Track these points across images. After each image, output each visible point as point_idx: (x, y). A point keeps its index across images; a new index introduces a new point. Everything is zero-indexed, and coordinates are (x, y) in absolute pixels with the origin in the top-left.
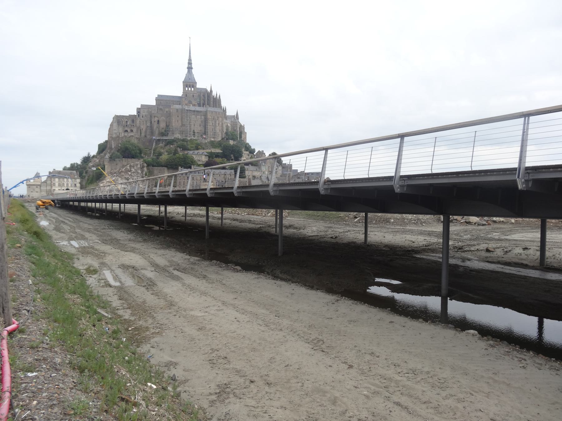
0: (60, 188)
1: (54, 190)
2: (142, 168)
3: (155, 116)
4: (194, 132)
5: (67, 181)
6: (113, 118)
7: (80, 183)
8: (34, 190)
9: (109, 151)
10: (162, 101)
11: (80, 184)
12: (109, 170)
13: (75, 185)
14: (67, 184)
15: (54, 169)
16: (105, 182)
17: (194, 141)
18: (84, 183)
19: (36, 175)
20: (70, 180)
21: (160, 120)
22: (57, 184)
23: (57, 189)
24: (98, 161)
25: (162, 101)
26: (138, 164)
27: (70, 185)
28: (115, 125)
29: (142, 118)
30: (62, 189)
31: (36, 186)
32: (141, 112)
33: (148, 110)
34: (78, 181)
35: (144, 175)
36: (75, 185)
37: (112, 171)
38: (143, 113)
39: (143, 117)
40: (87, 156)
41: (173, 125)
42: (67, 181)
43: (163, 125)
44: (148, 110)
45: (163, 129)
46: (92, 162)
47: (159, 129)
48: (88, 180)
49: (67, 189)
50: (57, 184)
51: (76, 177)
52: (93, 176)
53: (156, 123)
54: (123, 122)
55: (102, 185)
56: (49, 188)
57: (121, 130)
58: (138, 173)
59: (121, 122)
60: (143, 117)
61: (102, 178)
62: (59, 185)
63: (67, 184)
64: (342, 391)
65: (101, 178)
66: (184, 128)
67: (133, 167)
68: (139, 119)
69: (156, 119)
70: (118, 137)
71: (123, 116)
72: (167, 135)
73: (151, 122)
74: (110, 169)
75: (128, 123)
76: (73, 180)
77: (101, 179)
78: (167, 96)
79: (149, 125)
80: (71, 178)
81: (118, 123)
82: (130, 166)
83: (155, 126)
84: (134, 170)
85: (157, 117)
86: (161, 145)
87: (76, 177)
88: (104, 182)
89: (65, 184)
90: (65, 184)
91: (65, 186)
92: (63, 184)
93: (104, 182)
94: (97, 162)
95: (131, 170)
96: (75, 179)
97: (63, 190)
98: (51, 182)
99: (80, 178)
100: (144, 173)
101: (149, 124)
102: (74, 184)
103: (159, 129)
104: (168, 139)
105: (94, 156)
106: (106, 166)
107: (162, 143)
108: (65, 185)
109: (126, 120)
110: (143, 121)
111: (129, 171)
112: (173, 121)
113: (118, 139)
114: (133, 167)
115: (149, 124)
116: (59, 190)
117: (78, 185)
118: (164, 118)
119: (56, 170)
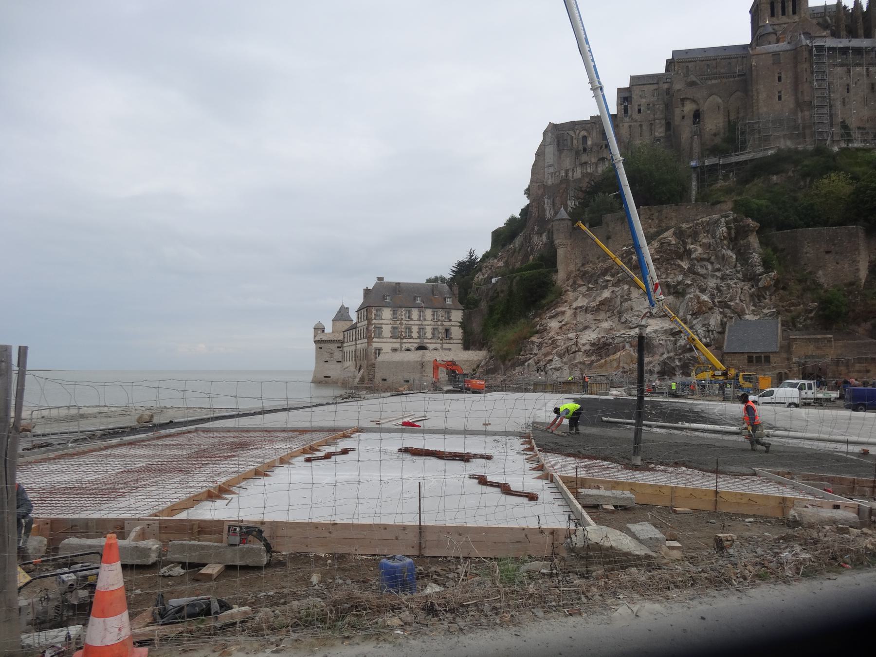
0: (397, 346)
1: (378, 351)
2: (736, 237)
3: (683, 100)
4: (844, 126)
5: (422, 318)
6: (545, 133)
7: (463, 325)
8: (331, 354)
9: (537, 228)
10: (690, 65)
11: (461, 330)
12: (572, 267)
13: (447, 330)
14: (421, 330)
15: (379, 279)
16: (569, 313)
17: (860, 154)
18: (476, 326)
19: (339, 312)
20: (429, 313)
21: (705, 107)
22: (387, 331)
23: (386, 348)
24: (501, 264)
25: (690, 65)
26: (717, 222)
27: (429, 334)
28: (550, 150)
29: (636, 116)
30: (405, 346)
31: (489, 428)
32: (635, 97)
33: (655, 87)
34: (457, 316)
35: (760, 269)
36: (447, 330)
37: (588, 268)
38: (639, 99)
39: (639, 111)
40: (465, 260)
41: (763, 110)
42: (422, 318)
43: (714, 124)
44: (655, 87)
45: (715, 135)
46: (484, 271)
47: (700, 136)
48: (491, 310)
49: (421, 348)
50: (387, 331)
51: (449, 302)
52: (511, 292)
53: (689, 121)
54: (575, 142)
55: (554, 324)
56: (362, 344)
57: (567, 163)
58: (724, 259)
59: (569, 141)
60: (639, 111)
61: (550, 297)
62: (396, 334)
63: (421, 330)
64: (620, 562)
65: (543, 297)
66: (807, 113)
67: (695, 236)
68: (627, 119)
69: (689, 107)
70: (565, 180)
71: (574, 123)
72: (741, 147)
73: (668, 125)
74: (579, 262)
75: (589, 143)
76: (440, 313)
77: (544, 302)
78: (705, 50)
79: (663, 135)
80: (434, 308)
81: (558, 145)
82: (680, 234)
83: (686, 131)
84: (700, 250)
85: (694, 101)
86: (721, 184)
87: (449, 302)
88: (563, 313)
89: (415, 329)
90: (415, 329)
91: (415, 335)
92: (408, 329)
93: (563, 313)
94: (498, 267)
95: (689, 253)
96: (448, 310)
97: (408, 350)
98: (369, 324)
99: (461, 307)
100: (756, 258)
101: (662, 129)
102: (441, 329)
103: (700, 136)
104: (751, 160)
105: (486, 256)
106: (561, 252)
107: (726, 177)
108: (415, 335)
109: (584, 133)
110: (641, 126)
111: (681, 257)
112: (763, 96)
113: (564, 186)
114: (695, 236)
115: (660, 132)
116: (394, 350)
117: (457, 332)
118: (720, 100)
119: (385, 280)
